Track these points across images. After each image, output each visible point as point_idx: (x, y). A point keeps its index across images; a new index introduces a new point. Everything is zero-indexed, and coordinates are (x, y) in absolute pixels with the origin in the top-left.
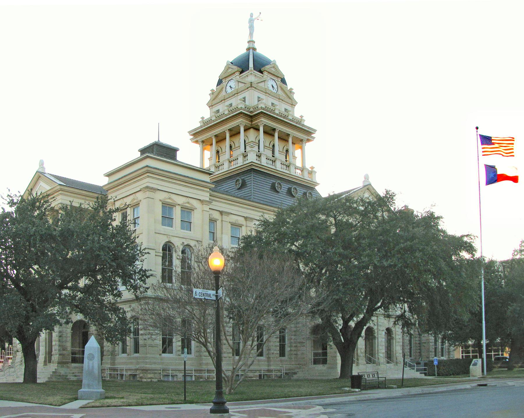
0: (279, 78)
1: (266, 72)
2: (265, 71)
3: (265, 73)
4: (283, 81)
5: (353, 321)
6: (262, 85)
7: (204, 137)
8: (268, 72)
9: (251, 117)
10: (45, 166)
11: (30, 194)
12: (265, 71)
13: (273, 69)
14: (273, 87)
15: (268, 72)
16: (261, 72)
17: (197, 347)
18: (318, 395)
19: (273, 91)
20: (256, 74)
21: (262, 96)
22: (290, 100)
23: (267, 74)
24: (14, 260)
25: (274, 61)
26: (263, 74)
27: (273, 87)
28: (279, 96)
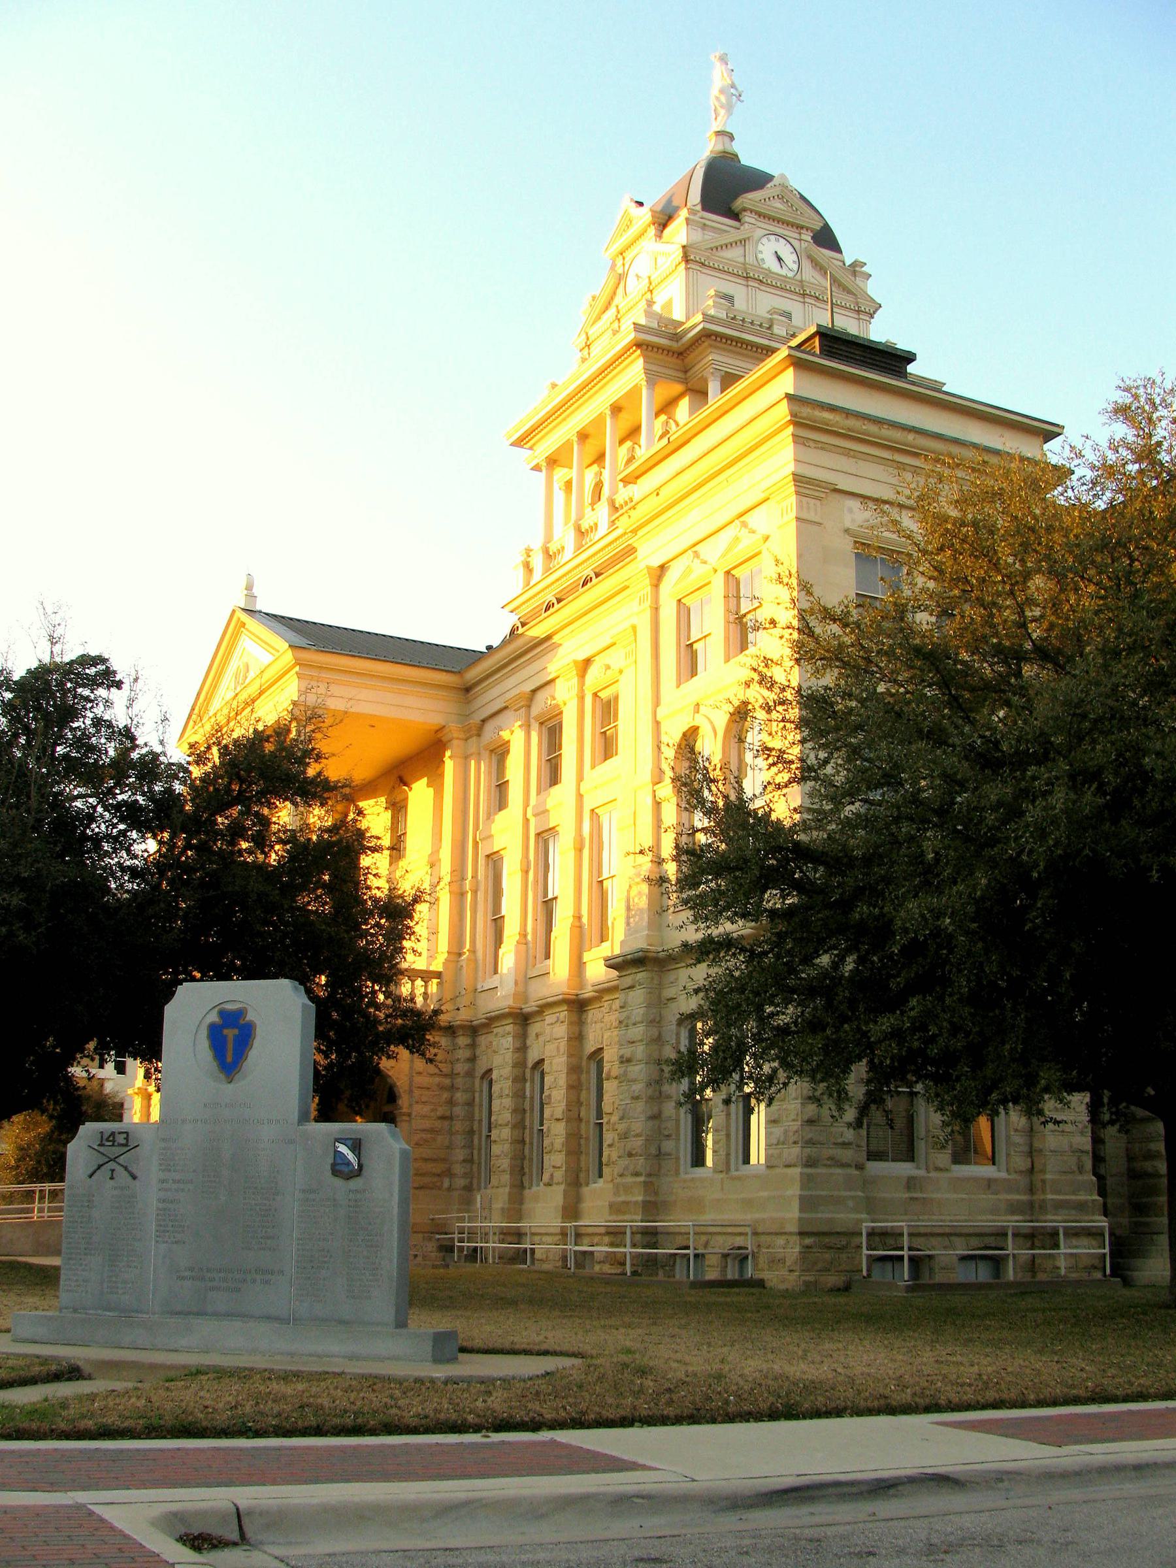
0: (804, 231)
1: (748, 213)
2: (745, 210)
3: (748, 218)
4: (826, 238)
5: (601, 1269)
6: (735, 254)
7: (547, 445)
8: (759, 214)
9: (680, 354)
10: (255, 591)
11: (802, 696)
12: (745, 210)
13: (778, 204)
14: (779, 259)
15: (759, 214)
16: (735, 216)
17: (810, 1122)
18: (1054, 1403)
19: (784, 272)
20: (708, 223)
21: (729, 287)
22: (850, 298)
23: (753, 221)
24: (312, 856)
25: (783, 176)
26: (739, 220)
27: (779, 259)
28: (745, 269)
